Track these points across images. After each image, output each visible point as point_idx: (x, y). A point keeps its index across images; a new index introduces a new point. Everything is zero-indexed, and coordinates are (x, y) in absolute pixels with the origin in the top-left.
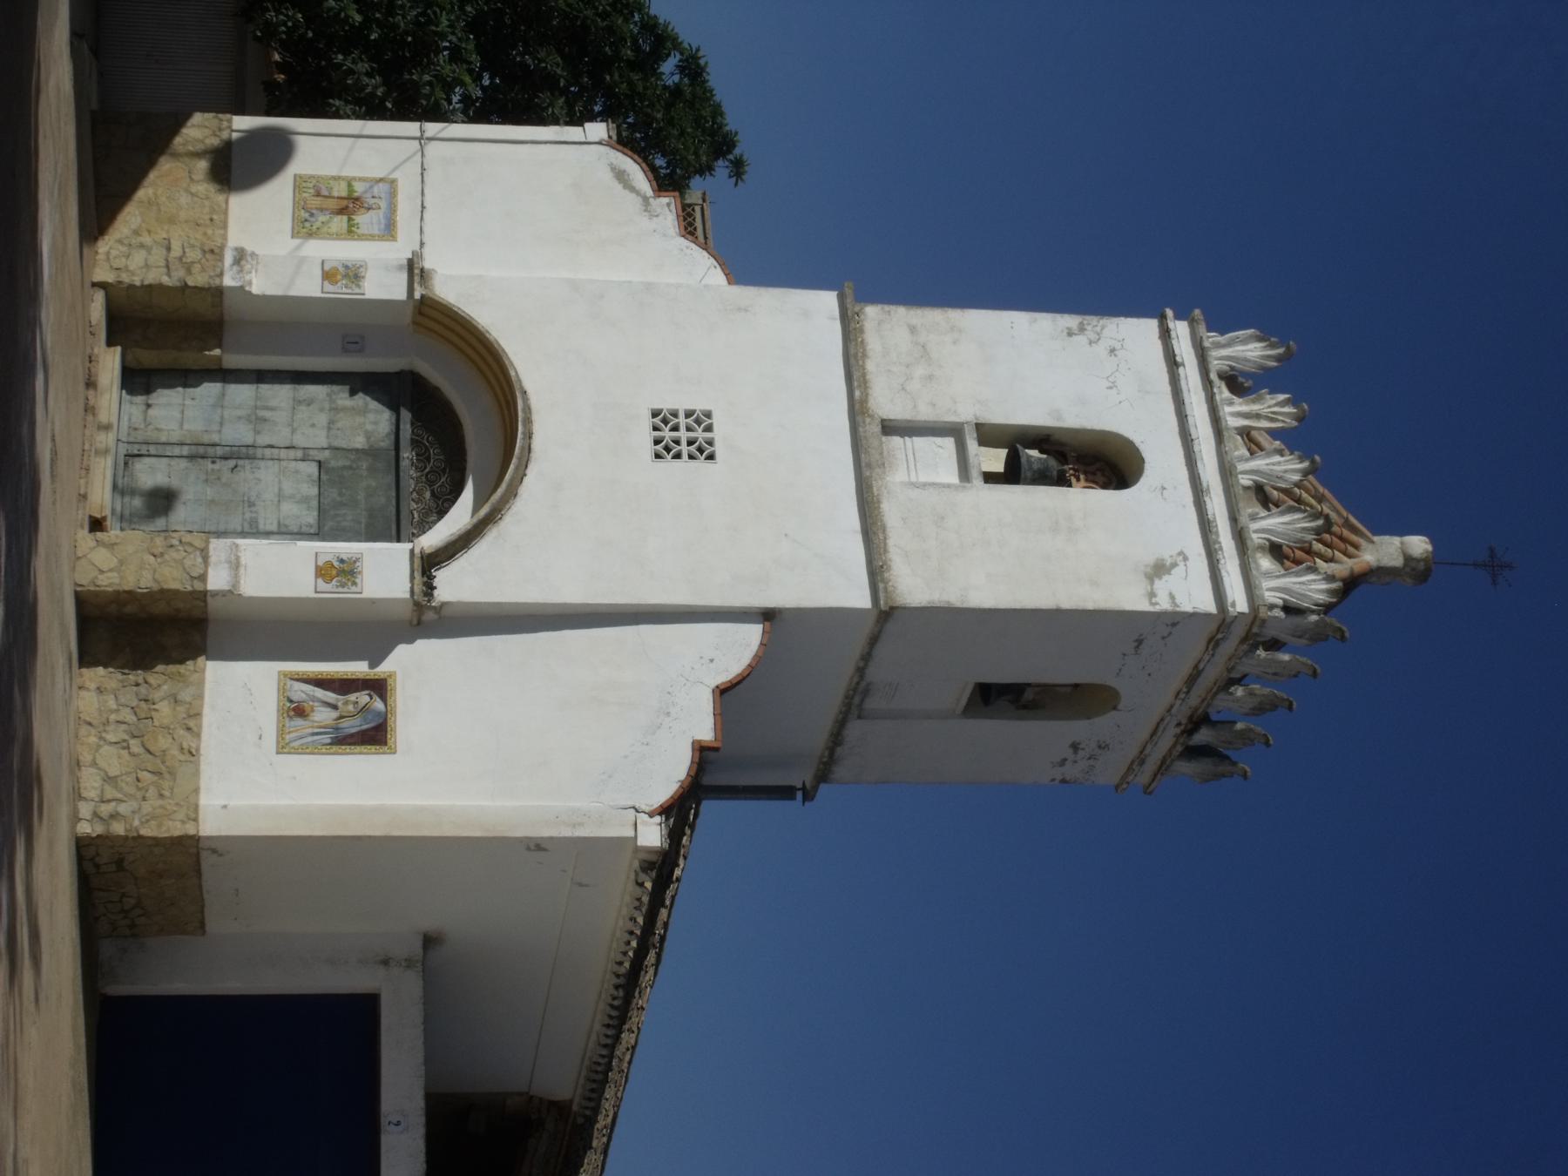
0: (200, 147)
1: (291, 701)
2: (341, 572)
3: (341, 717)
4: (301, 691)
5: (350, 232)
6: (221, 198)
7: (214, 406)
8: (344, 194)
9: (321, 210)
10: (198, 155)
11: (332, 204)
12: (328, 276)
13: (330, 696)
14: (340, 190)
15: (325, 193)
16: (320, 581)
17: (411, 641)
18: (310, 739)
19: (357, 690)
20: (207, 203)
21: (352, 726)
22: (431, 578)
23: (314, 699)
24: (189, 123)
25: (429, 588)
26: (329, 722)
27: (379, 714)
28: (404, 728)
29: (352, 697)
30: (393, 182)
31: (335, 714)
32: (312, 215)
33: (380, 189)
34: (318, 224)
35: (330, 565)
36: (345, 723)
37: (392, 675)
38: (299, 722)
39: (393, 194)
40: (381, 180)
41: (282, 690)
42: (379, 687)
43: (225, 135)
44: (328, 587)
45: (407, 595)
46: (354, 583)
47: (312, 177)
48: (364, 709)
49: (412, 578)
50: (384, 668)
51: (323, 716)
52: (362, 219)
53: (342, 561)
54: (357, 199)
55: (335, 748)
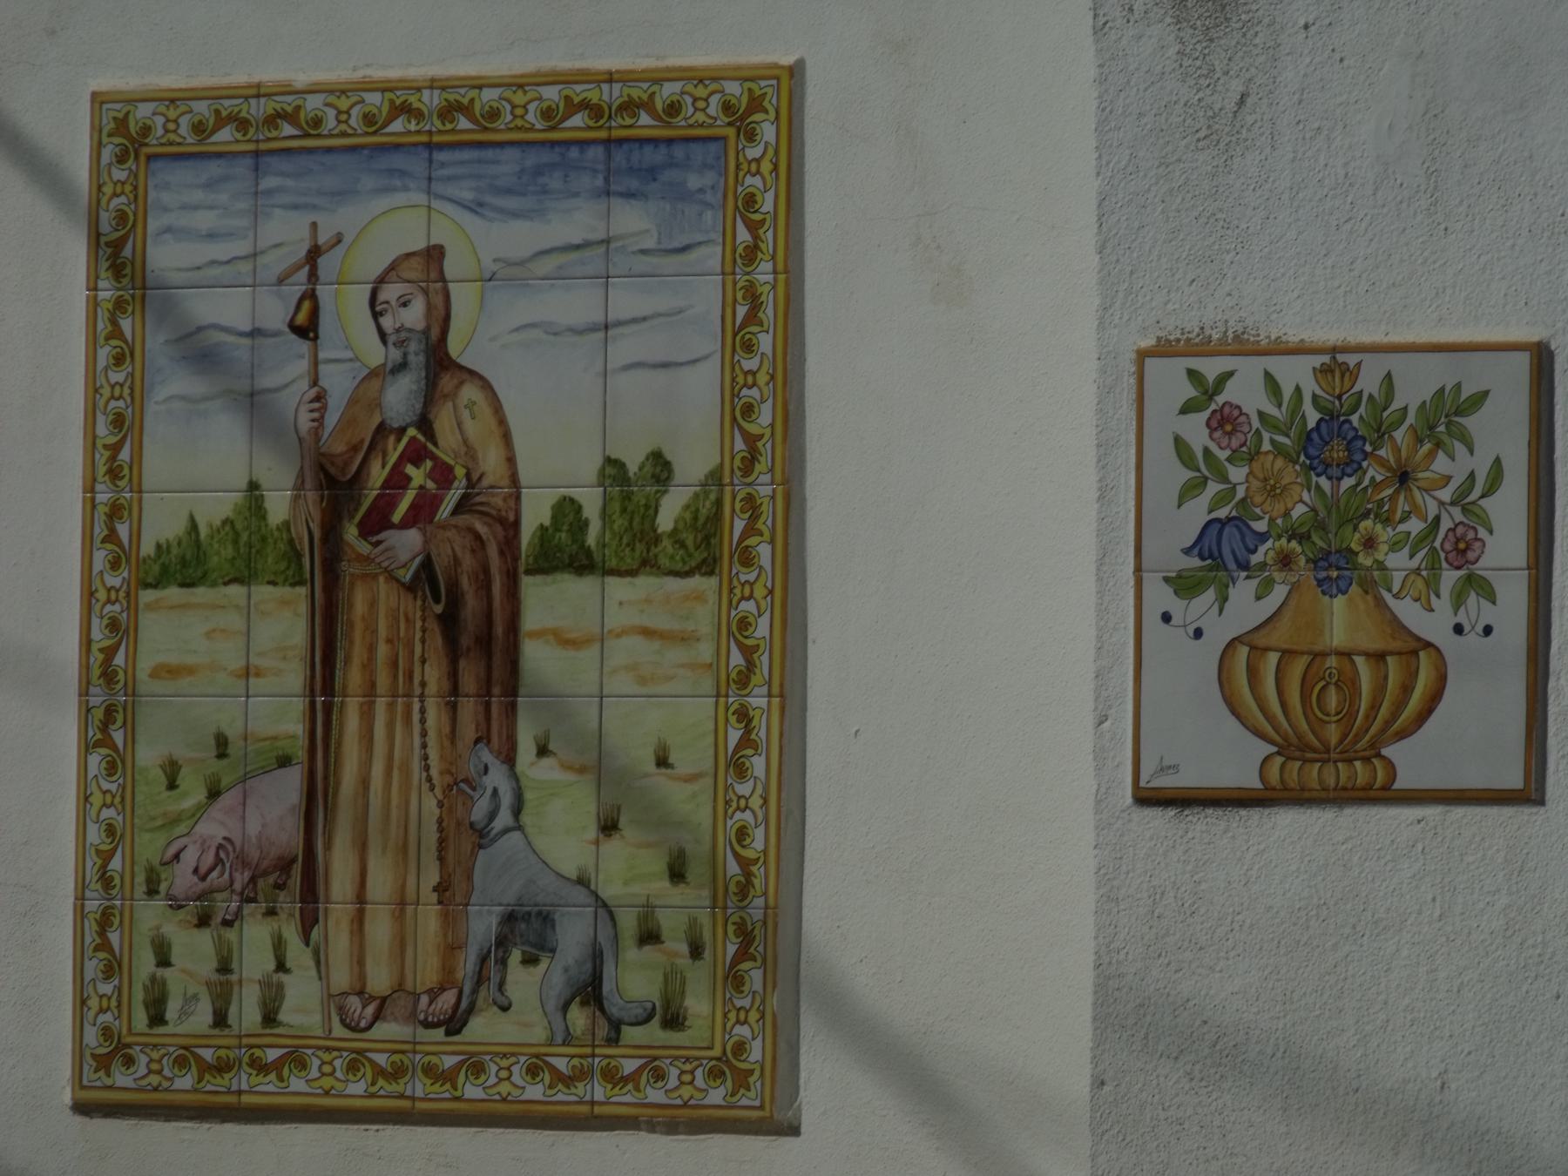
5: (703, 549)
7: (482, 836)
8: (281, 621)
9: (464, 838)
11: (393, 751)
14: (237, 657)
15: (270, 815)
16: (1411, 761)
30: (135, 140)
32: (526, 929)
34: (628, 871)
39: (267, 135)
40: (116, 252)
45: (245, 927)
46: (1448, 415)
47: (100, 934)
52: (563, 404)
54: (332, 482)
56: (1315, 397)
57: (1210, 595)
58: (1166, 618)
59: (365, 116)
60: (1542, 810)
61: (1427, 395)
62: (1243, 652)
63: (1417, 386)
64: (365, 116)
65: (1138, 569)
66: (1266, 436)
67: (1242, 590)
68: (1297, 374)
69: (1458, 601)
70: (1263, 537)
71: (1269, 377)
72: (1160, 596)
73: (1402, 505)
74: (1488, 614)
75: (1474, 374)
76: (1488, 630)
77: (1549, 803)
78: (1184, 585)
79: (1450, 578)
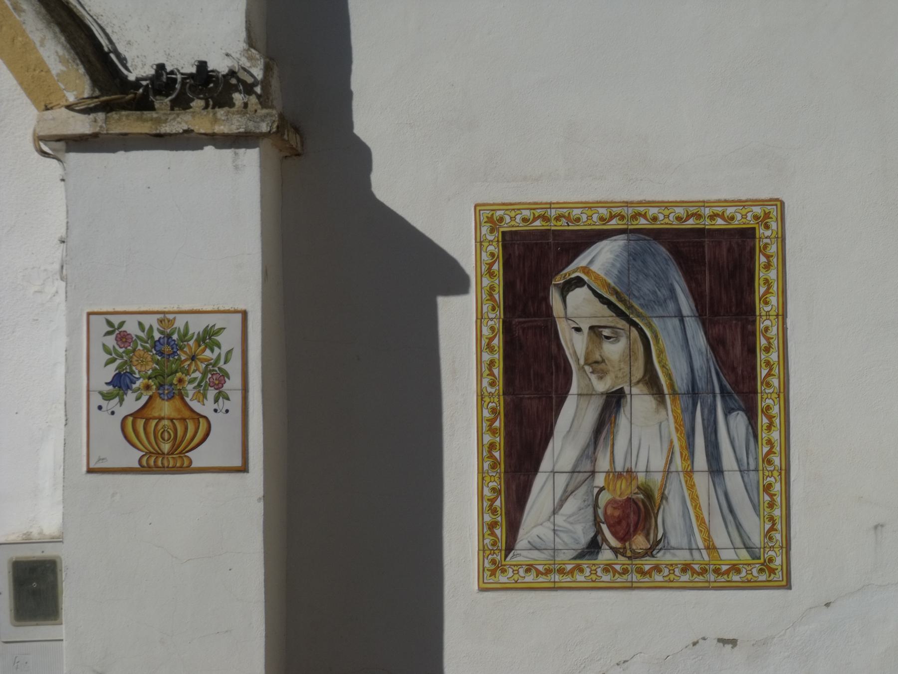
1: (594, 547)
2: (165, 384)
3: (651, 381)
4: (554, 513)
12: (165, 447)
13: (573, 419)
16: (198, 457)
17: (360, 157)
18: (733, 481)
19: (549, 330)
21: (682, 344)
22: (162, 82)
23: (584, 470)
25: (207, 86)
26: (669, 419)
27: (634, 259)
28: (690, 172)
29: (575, 345)
31: (640, 403)
35: (129, 428)
36: (674, 367)
37: (488, 216)
38: (671, 518)
41: (551, 576)
42: (534, 258)
44: (224, 429)
45: (251, 157)
46: (209, 337)
48: (618, 305)
49: (188, 141)
50: (461, 240)
51: (647, 438)
53: (121, 383)
55: (766, 399)
56: (158, 329)
57: (117, 400)
58: (100, 408)
59: (770, 484)
60: (248, 475)
61: (201, 330)
62: (130, 419)
63: (197, 326)
64: (770, 484)
65: (88, 391)
66: (139, 342)
67: (130, 397)
68: (151, 321)
69: (216, 401)
70: (138, 379)
71: (140, 324)
72: (97, 400)
73: (193, 367)
74: (227, 405)
75: (218, 321)
76: (227, 411)
77: (793, 588)
78: (107, 397)
79: (212, 393)
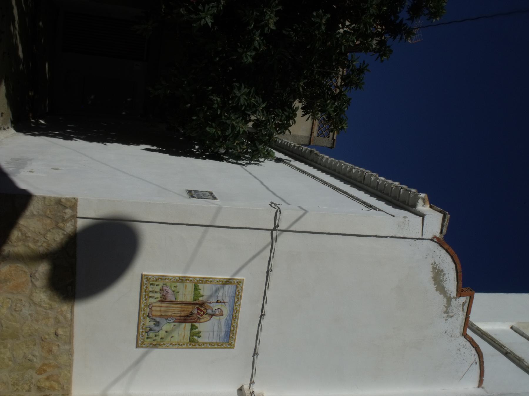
0: (41, 247)
5: (192, 341)
6: (65, 307)
8: (189, 298)
10: (37, 258)
11: (175, 310)
14: (186, 294)
15: (171, 297)
20: (51, 314)
24: (28, 213)
32: (157, 324)
33: (229, 289)
34: (162, 334)
39: (236, 298)
40: (228, 282)
43: (69, 228)
54: (202, 304)
